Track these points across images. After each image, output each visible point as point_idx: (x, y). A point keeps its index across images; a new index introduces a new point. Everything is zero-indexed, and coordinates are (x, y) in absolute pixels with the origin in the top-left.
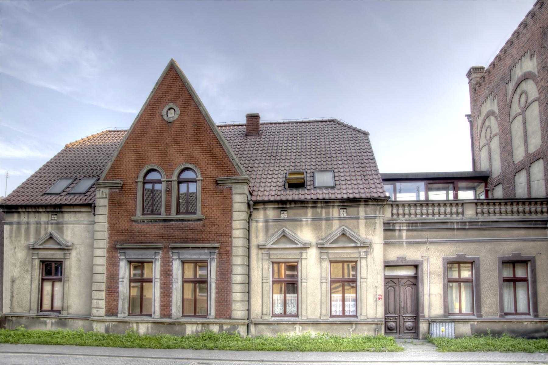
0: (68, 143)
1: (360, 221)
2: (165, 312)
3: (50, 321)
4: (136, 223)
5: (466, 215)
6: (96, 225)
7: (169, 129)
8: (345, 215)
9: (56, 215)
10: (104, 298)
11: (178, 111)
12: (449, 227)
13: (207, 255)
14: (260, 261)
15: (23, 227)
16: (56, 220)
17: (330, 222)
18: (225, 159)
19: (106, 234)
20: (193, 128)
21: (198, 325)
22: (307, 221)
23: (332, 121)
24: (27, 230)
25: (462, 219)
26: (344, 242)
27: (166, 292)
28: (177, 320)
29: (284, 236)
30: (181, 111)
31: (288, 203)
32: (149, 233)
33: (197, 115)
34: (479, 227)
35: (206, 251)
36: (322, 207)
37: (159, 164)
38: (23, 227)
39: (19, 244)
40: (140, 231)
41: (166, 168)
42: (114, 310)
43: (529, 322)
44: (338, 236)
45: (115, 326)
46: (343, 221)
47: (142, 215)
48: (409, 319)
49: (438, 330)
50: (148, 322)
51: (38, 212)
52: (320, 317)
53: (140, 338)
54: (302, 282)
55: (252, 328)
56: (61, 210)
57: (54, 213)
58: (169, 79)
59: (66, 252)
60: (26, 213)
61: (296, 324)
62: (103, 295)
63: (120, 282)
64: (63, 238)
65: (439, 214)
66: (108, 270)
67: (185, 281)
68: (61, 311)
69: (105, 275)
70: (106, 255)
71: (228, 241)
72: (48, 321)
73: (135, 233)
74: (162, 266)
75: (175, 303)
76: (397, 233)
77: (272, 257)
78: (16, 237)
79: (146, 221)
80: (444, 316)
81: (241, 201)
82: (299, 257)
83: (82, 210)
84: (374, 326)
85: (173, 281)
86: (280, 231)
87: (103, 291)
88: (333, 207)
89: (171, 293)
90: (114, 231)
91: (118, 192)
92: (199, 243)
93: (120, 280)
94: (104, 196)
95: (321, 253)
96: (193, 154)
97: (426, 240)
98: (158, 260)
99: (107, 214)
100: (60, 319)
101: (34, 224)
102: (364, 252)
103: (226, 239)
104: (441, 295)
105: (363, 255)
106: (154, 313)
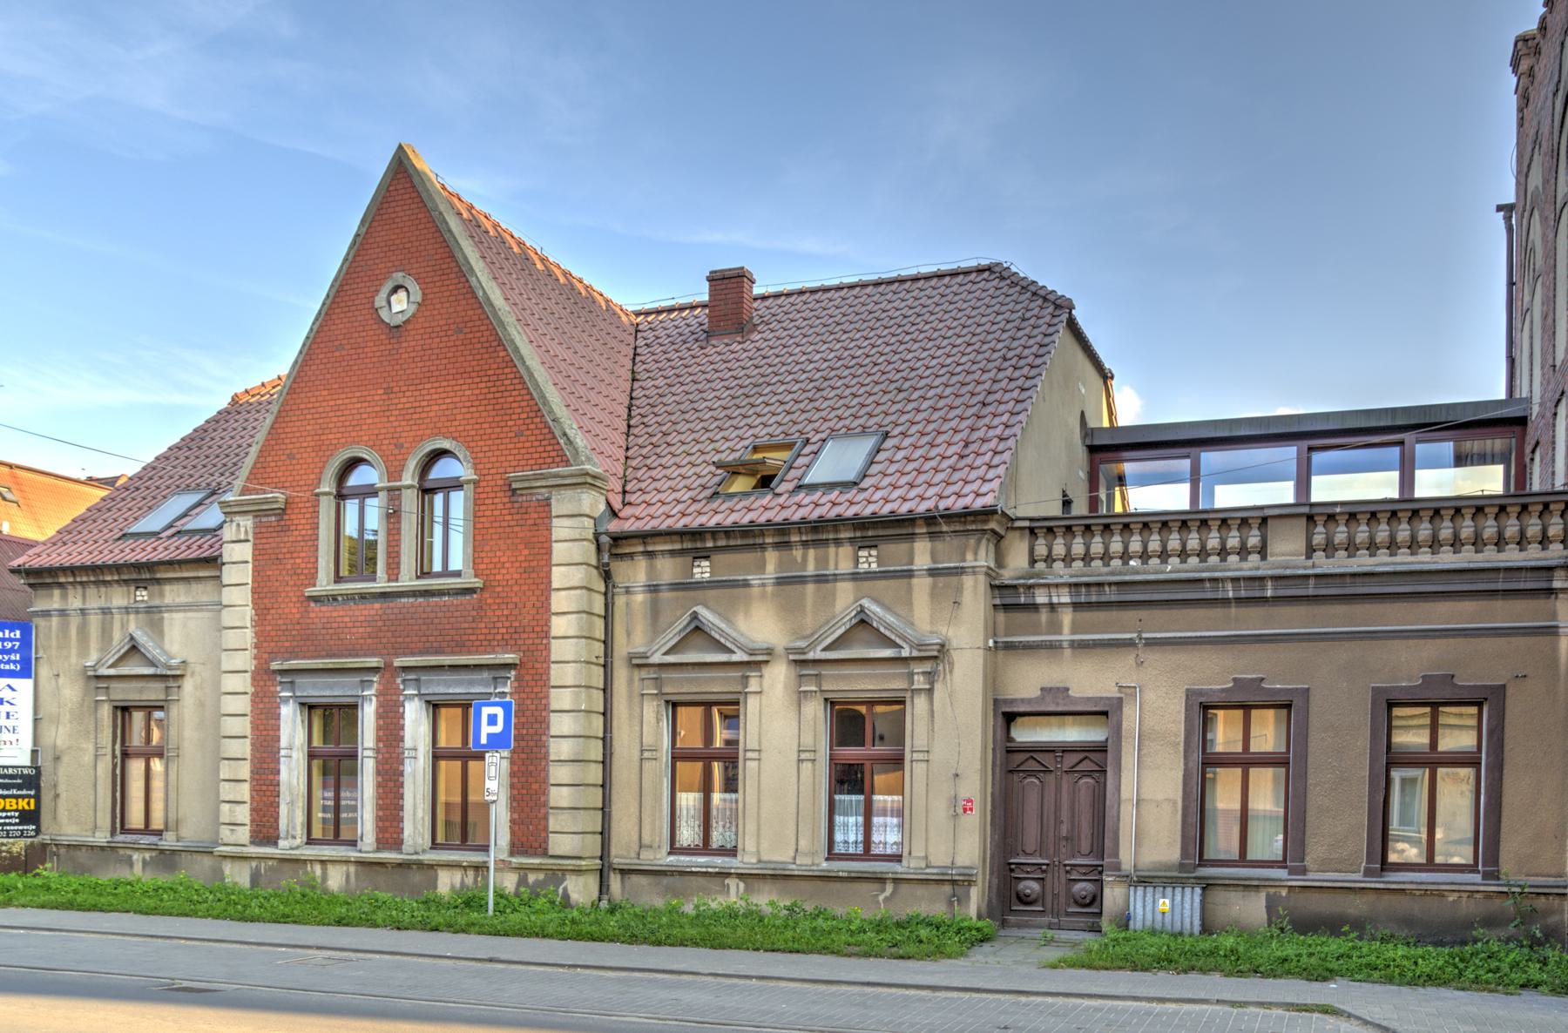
0: (240, 390)
1: (915, 581)
2: (387, 835)
3: (141, 856)
4: (318, 604)
5: (1271, 556)
6: (225, 612)
7: (396, 346)
8: (874, 566)
9: (145, 588)
10: (247, 797)
11: (417, 296)
12: (1209, 595)
13: (487, 685)
14: (637, 700)
15: (74, 622)
16: (146, 602)
17: (829, 586)
18: (535, 420)
19: (248, 637)
20: (454, 338)
21: (466, 871)
22: (763, 585)
23: (989, 269)
24: (83, 631)
25: (1258, 569)
26: (869, 645)
27: (391, 784)
28: (415, 857)
29: (697, 628)
30: (424, 294)
31: (708, 536)
32: (346, 630)
33: (464, 302)
34: (1311, 592)
35: (486, 675)
36: (805, 544)
37: (371, 443)
38: (74, 622)
39: (66, 664)
40: (329, 626)
41: (386, 453)
42: (271, 830)
43: (1465, 895)
44: (848, 627)
45: (271, 869)
46: (867, 584)
47: (335, 582)
48: (1085, 874)
49: (1149, 908)
50: (347, 862)
51: (105, 583)
52: (795, 858)
53: (333, 899)
54: (745, 760)
55: (615, 882)
56: (152, 576)
57: (140, 584)
58: (394, 204)
59: (171, 683)
60: (79, 588)
61: (728, 875)
62: (244, 791)
63: (282, 759)
64: (162, 648)
65: (1183, 554)
66: (255, 727)
67: (437, 756)
68: (164, 833)
69: (248, 742)
70: (250, 689)
71: (540, 647)
72: (136, 856)
73: (317, 632)
74: (379, 716)
75: (412, 812)
76: (1044, 616)
77: (667, 689)
78: (59, 648)
79: (340, 598)
80: (1182, 867)
81: (573, 537)
82: (739, 689)
83: (201, 574)
84: (947, 889)
85: (406, 755)
86: (686, 619)
87: (245, 781)
88: (838, 542)
89: (402, 785)
90: (268, 628)
91: (275, 524)
92: (469, 653)
93: (283, 753)
94: (242, 537)
95: (801, 676)
96: (455, 411)
97: (1135, 635)
98: (371, 700)
99: (250, 582)
100: (162, 851)
101: (96, 614)
102: (923, 673)
103: (537, 641)
104: (1175, 803)
105: (920, 682)
106: (362, 840)
